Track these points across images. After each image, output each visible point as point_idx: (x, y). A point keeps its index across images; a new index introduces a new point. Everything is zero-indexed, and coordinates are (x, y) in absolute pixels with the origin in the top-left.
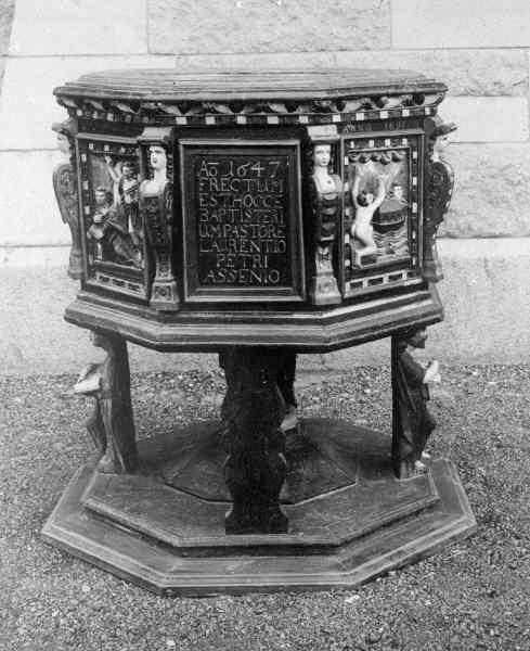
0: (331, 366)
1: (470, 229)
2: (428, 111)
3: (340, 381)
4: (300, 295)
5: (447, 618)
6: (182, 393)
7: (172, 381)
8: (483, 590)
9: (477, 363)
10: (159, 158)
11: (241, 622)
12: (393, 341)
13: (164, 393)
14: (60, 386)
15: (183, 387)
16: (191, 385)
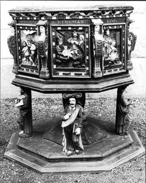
0: (91, 97)
1: (136, 55)
2: (127, 15)
3: (94, 102)
4: (90, 76)
5: (126, 177)
6: (45, 105)
7: (41, 101)
8: (138, 168)
9: (137, 97)
10: (43, 29)
11: (61, 177)
12: (118, 92)
13: (39, 105)
14: (6, 102)
15: (45, 103)
16: (47, 103)
